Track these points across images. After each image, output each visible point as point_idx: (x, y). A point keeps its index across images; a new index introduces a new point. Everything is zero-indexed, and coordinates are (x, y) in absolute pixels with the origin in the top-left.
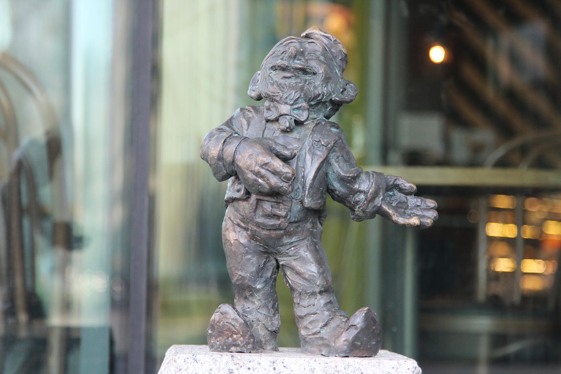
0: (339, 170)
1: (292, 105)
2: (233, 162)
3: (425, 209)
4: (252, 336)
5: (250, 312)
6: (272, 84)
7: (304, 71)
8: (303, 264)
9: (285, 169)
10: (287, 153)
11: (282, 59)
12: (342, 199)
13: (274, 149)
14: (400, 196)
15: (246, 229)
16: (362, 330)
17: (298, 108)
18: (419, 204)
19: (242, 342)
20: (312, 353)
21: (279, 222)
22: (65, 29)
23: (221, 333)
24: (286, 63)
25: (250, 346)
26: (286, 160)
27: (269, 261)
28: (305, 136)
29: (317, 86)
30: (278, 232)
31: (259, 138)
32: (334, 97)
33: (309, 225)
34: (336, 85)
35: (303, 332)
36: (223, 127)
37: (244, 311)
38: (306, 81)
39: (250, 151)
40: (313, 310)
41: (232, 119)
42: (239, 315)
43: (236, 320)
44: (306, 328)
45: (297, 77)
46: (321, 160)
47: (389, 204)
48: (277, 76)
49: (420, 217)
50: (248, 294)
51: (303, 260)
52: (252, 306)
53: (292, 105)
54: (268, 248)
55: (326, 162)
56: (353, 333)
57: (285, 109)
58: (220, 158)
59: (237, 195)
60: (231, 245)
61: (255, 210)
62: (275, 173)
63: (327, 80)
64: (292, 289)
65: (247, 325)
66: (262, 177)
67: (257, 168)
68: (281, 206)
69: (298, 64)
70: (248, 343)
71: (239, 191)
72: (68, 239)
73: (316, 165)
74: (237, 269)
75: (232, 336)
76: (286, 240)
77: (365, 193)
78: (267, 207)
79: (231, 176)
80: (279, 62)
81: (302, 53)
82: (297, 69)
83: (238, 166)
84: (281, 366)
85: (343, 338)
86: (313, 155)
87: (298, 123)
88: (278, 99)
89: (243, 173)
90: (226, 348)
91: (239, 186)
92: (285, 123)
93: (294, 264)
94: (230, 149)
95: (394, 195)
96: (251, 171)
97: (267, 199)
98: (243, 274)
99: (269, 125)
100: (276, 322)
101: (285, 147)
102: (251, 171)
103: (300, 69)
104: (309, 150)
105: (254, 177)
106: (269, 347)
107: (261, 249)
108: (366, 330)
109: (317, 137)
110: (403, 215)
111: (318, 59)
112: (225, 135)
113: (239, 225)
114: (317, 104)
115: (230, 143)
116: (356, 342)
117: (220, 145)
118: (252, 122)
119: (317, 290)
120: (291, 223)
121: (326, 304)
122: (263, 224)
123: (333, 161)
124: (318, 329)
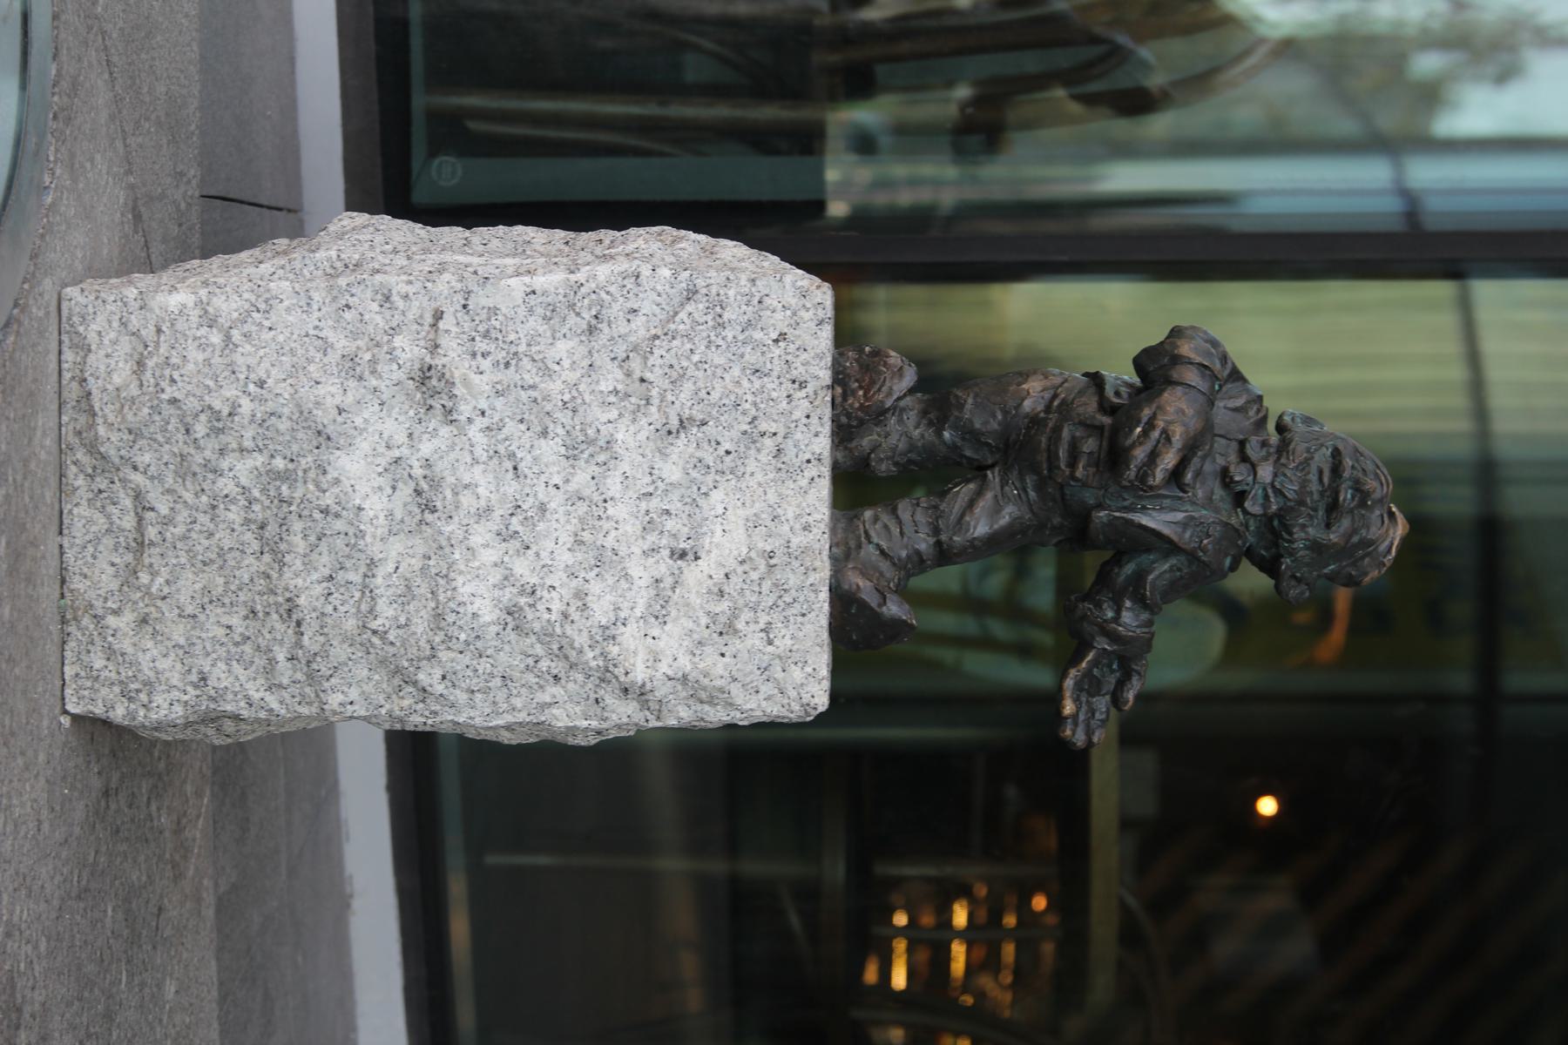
0: (1156, 573)
1: (1273, 486)
2: (1170, 382)
3: (1088, 726)
4: (862, 423)
5: (900, 421)
6: (1308, 450)
7: (1333, 507)
8: (986, 513)
9: (1159, 475)
10: (1189, 476)
11: (1353, 467)
12: (1104, 577)
13: (1195, 454)
14: (1112, 680)
15: (1048, 409)
16: (876, 615)
17: (1266, 497)
18: (1097, 715)
19: (851, 405)
20: (833, 531)
21: (1063, 466)
22: (1274, 142)
24: (1346, 474)
25: (844, 420)
26: (1176, 476)
27: (992, 453)
28: (1217, 510)
29: (1307, 531)
30: (1045, 466)
31: (1212, 427)
32: (1287, 562)
33: (1057, 520)
34: (1307, 565)
35: (868, 514)
36: (1229, 365)
37: (903, 410)
38: (1315, 510)
39: (1190, 412)
41: (1244, 380)
42: (899, 399)
43: (889, 394)
44: (876, 519)
45: (1322, 493)
46: (1175, 538)
47: (1095, 663)
48: (1322, 458)
49: (1075, 717)
50: (932, 416)
51: (997, 510)
52: (911, 423)
53: (1273, 486)
55: (1166, 546)
56: (871, 599)
57: (1265, 472)
58: (1177, 360)
59: (1109, 391)
60: (1019, 384)
61: (1082, 424)
62: (1153, 456)
63: (1316, 547)
65: (879, 415)
66: (1145, 433)
67: (1161, 424)
68: (1092, 470)
69: (1346, 495)
70: (848, 415)
71: (1117, 394)
72: (980, 132)
73: (1166, 531)
74: (976, 395)
75: (861, 387)
76: (1030, 480)
77: (1116, 619)
79: (1143, 380)
80: (1348, 462)
81: (1363, 504)
82: (1337, 493)
83: (1163, 390)
84: (814, 473)
86: (1185, 525)
87: (1239, 498)
88: (1283, 461)
89: (1150, 400)
90: (840, 378)
91: (1125, 396)
92: (1239, 474)
93: (989, 495)
94: (1192, 377)
95: (1112, 671)
96: (1155, 414)
97: (1105, 444)
98: (968, 406)
99: (1234, 445)
100: (883, 467)
101: (1198, 474)
102: (1155, 414)
103: (1336, 499)
104: (1192, 518)
105: (1145, 419)
106: (839, 456)
107: (1013, 437)
109: (1216, 531)
110: (1078, 687)
111: (1355, 531)
112: (1217, 366)
113: (1055, 396)
114: (1272, 530)
115: (1203, 376)
117: (1198, 359)
118: (1239, 416)
119: (944, 537)
120: (1062, 487)
121: (918, 553)
122: (1059, 438)
123: (1173, 561)
124: (875, 540)
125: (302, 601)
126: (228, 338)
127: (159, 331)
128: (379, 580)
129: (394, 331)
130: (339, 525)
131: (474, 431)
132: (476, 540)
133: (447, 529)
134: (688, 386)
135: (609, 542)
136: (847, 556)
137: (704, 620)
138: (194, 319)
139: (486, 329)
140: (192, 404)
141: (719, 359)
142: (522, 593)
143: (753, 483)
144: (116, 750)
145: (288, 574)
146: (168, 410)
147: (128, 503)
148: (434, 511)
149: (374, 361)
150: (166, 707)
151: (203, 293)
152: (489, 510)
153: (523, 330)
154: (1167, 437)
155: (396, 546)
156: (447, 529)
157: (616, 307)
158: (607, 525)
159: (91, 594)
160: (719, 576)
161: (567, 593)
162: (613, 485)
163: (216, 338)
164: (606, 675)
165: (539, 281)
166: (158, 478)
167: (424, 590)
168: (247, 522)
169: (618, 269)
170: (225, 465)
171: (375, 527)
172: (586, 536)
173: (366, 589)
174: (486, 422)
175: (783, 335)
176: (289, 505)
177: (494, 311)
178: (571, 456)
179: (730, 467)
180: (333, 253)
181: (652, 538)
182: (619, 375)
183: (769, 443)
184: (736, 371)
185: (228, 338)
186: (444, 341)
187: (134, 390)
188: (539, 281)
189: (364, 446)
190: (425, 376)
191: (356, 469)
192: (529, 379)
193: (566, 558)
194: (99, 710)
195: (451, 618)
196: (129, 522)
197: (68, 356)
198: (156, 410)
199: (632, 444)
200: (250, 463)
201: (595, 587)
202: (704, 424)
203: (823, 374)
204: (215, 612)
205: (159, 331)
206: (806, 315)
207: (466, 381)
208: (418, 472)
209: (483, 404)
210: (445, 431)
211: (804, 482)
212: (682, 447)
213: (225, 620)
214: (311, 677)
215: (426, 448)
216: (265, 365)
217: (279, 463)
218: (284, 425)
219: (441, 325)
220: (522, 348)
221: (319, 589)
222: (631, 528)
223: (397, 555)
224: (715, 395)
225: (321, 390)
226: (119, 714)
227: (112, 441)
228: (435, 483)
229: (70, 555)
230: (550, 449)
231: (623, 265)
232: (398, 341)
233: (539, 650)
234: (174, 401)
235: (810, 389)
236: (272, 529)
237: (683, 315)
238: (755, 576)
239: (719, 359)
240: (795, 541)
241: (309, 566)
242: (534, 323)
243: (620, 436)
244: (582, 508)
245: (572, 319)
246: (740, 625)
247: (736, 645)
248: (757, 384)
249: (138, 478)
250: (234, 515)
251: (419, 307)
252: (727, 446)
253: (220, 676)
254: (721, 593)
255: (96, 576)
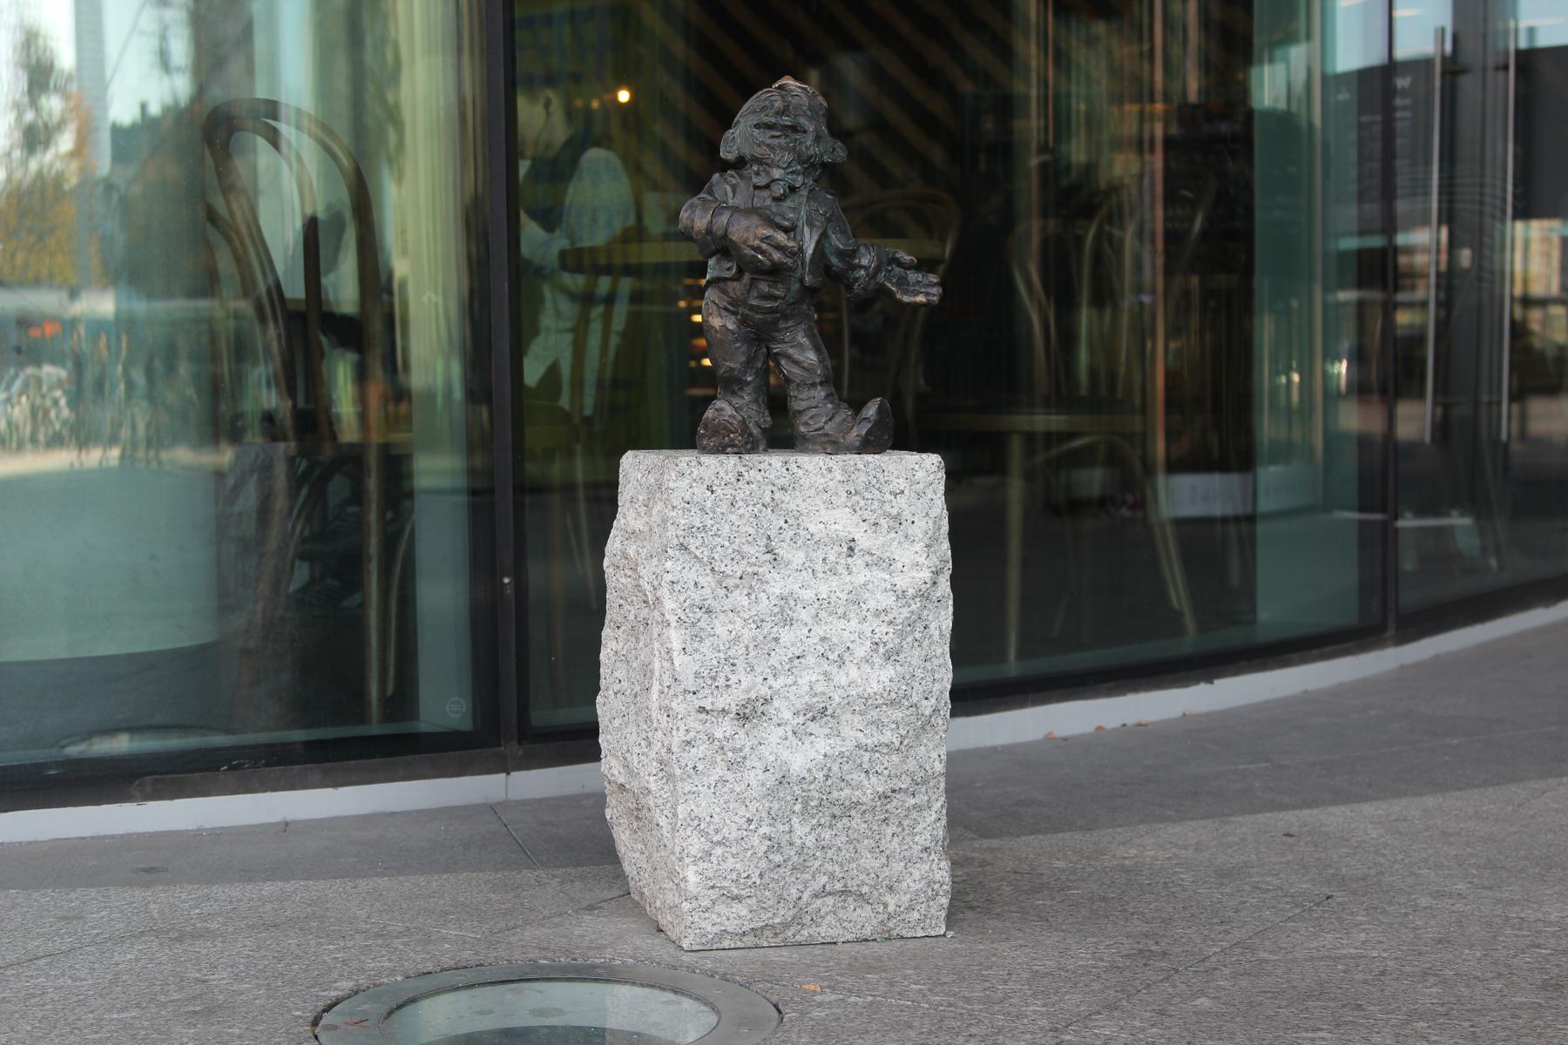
2: (725, 236)
7: (794, 129)
8: (802, 353)
15: (733, 313)
20: (815, 452)
23: (715, 433)
40: (813, 405)
44: (806, 424)
48: (762, 136)
49: (927, 294)
51: (800, 346)
54: (760, 334)
55: (824, 236)
56: (866, 427)
57: (777, 173)
58: (709, 231)
59: (727, 275)
62: (779, 247)
63: (818, 139)
64: (788, 380)
66: (763, 252)
67: (757, 242)
69: (786, 120)
73: (816, 237)
76: (782, 325)
77: (865, 268)
78: (764, 287)
80: (766, 119)
85: (854, 433)
87: (793, 189)
92: (779, 190)
93: (791, 351)
108: (878, 424)
109: (814, 205)
110: (906, 292)
116: (1084, 390)
121: (827, 397)
125: (881, 790)
126: (719, 843)
127: (713, 887)
128: (869, 741)
129: (711, 738)
130: (835, 768)
131: (777, 685)
132: (844, 681)
133: (837, 700)
134: (745, 548)
135: (844, 596)
136: (835, 443)
137: (893, 535)
138: (706, 865)
139: (711, 678)
140: (763, 864)
141: (726, 529)
142: (876, 651)
143: (803, 505)
144: (969, 901)
145: (864, 799)
146: (766, 880)
147: (819, 902)
148: (825, 709)
149: (734, 750)
150: (941, 872)
151: (687, 860)
152: (825, 674)
153: (710, 655)
154: (766, 239)
155: (846, 731)
156: (837, 700)
157: (694, 596)
158: (833, 599)
159: (874, 922)
160: (865, 526)
161: (876, 622)
162: (808, 595)
163: (719, 851)
164: (924, 596)
165: (676, 645)
166: (805, 883)
167: (875, 713)
168: (831, 827)
169: (667, 595)
170: (799, 842)
171: (838, 746)
172: (841, 611)
173: (875, 749)
174: (770, 677)
175: (710, 488)
176: (824, 801)
177: (697, 675)
178: (789, 622)
179: (793, 520)
180: (652, 779)
181: (840, 569)
182: (737, 592)
183: (777, 496)
184: (733, 517)
185: (719, 843)
186: (720, 706)
187: (754, 900)
188: (676, 645)
189: (785, 755)
190: (742, 718)
191: (800, 759)
192: (742, 651)
193: (854, 623)
194: (943, 914)
195: (893, 695)
196: (830, 900)
197: (726, 944)
198: (766, 887)
199: (782, 583)
200: (797, 826)
201: (872, 604)
202: (769, 538)
203: (731, 461)
204: (884, 844)
205: (713, 887)
206: (696, 473)
207: (748, 691)
208: (801, 719)
209: (760, 679)
210: (776, 703)
211: (801, 472)
212: (784, 551)
213: (889, 838)
214: (925, 782)
215: (787, 715)
216: (736, 819)
217: (798, 807)
218: (776, 806)
219: (709, 708)
220: (722, 655)
221: (874, 779)
222: (834, 582)
223: (852, 731)
224: (751, 531)
225: (754, 783)
226: (945, 901)
227: (784, 913)
228: (809, 708)
229: (850, 937)
230: (786, 635)
231: (664, 592)
232: (719, 735)
233: (910, 639)
234: (761, 875)
235: (743, 470)
236: (836, 810)
237: (698, 553)
238: (862, 503)
239: (726, 529)
240: (839, 477)
241: (859, 786)
242: (705, 648)
243: (778, 591)
244: (823, 614)
245: (702, 624)
246: (894, 512)
247: (906, 514)
248: (741, 504)
249: (806, 896)
250: (827, 834)
251: (694, 722)
252: (782, 523)
253: (923, 839)
254: (876, 524)
255: (863, 919)
